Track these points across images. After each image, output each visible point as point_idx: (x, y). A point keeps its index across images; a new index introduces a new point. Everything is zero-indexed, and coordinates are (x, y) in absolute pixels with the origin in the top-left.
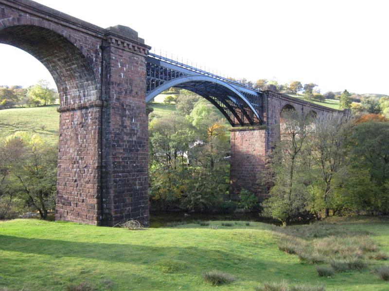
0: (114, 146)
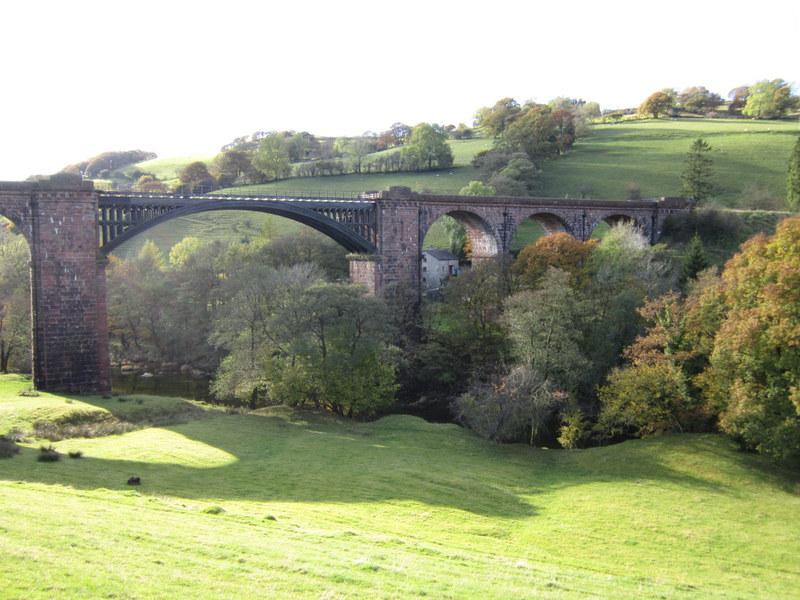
0: (46, 309)
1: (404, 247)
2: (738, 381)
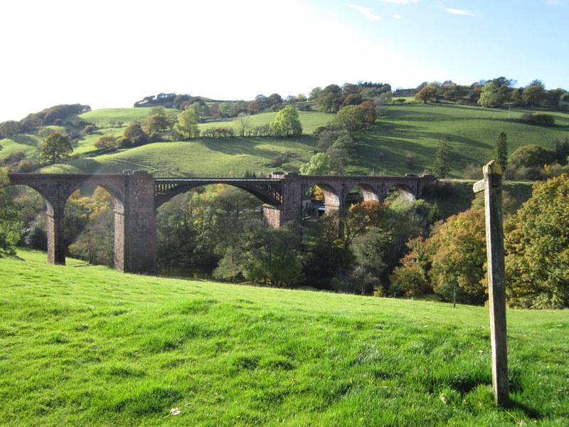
1: (294, 203)
2: (441, 274)
